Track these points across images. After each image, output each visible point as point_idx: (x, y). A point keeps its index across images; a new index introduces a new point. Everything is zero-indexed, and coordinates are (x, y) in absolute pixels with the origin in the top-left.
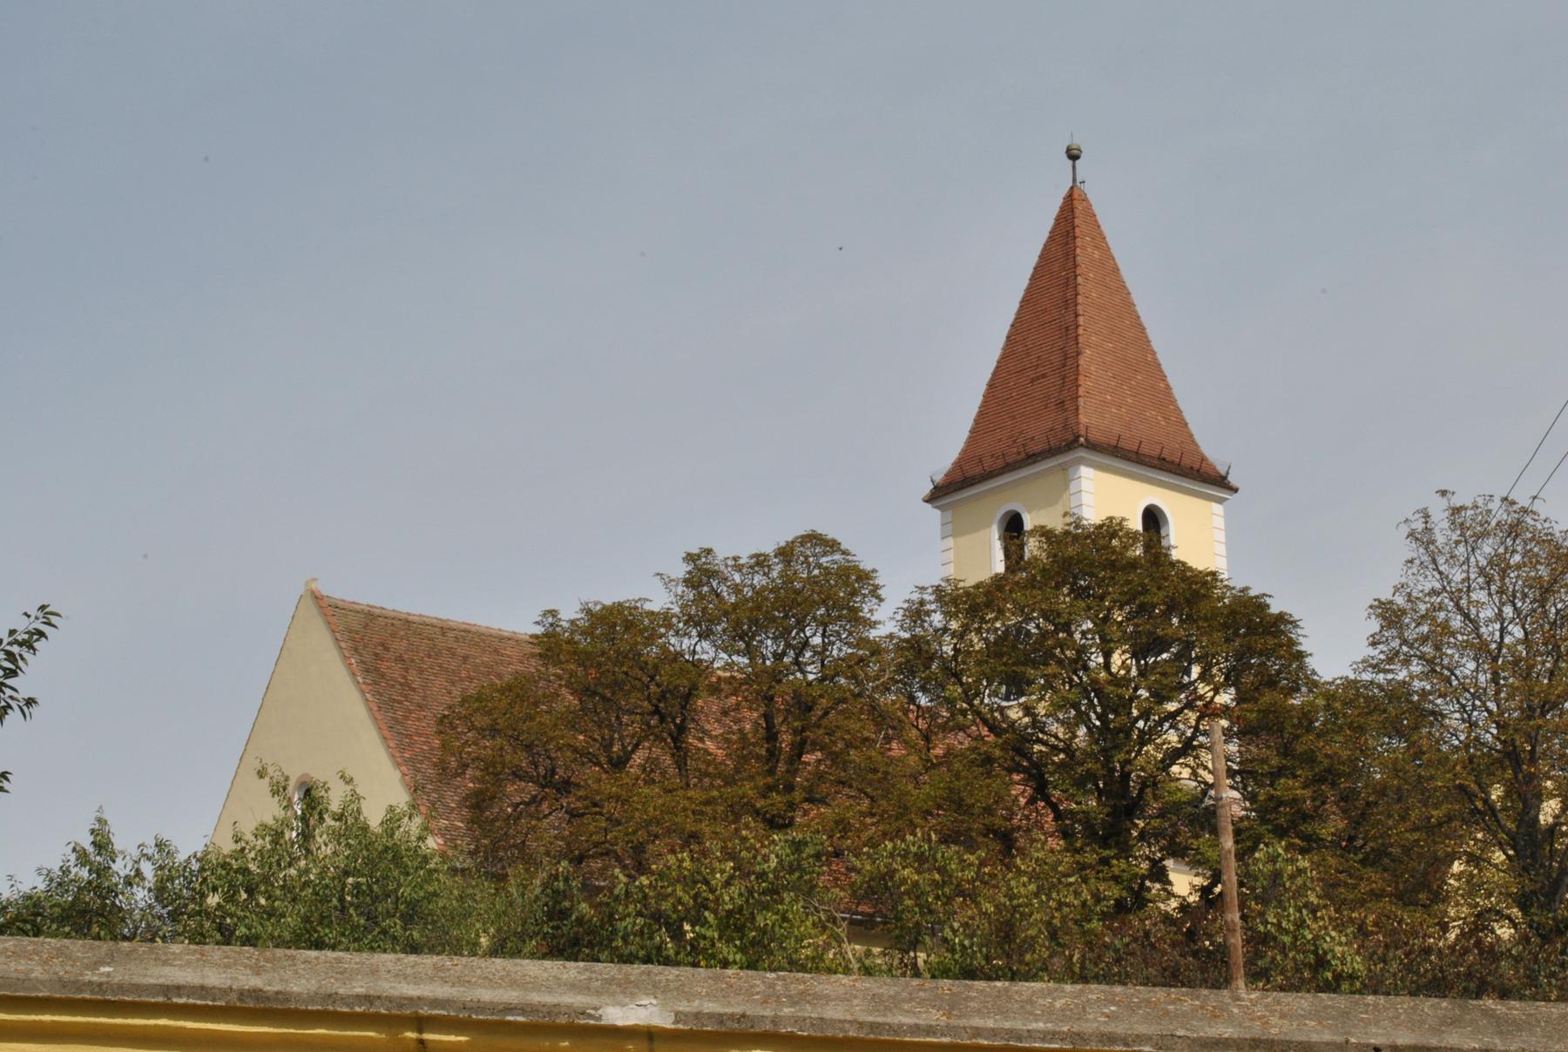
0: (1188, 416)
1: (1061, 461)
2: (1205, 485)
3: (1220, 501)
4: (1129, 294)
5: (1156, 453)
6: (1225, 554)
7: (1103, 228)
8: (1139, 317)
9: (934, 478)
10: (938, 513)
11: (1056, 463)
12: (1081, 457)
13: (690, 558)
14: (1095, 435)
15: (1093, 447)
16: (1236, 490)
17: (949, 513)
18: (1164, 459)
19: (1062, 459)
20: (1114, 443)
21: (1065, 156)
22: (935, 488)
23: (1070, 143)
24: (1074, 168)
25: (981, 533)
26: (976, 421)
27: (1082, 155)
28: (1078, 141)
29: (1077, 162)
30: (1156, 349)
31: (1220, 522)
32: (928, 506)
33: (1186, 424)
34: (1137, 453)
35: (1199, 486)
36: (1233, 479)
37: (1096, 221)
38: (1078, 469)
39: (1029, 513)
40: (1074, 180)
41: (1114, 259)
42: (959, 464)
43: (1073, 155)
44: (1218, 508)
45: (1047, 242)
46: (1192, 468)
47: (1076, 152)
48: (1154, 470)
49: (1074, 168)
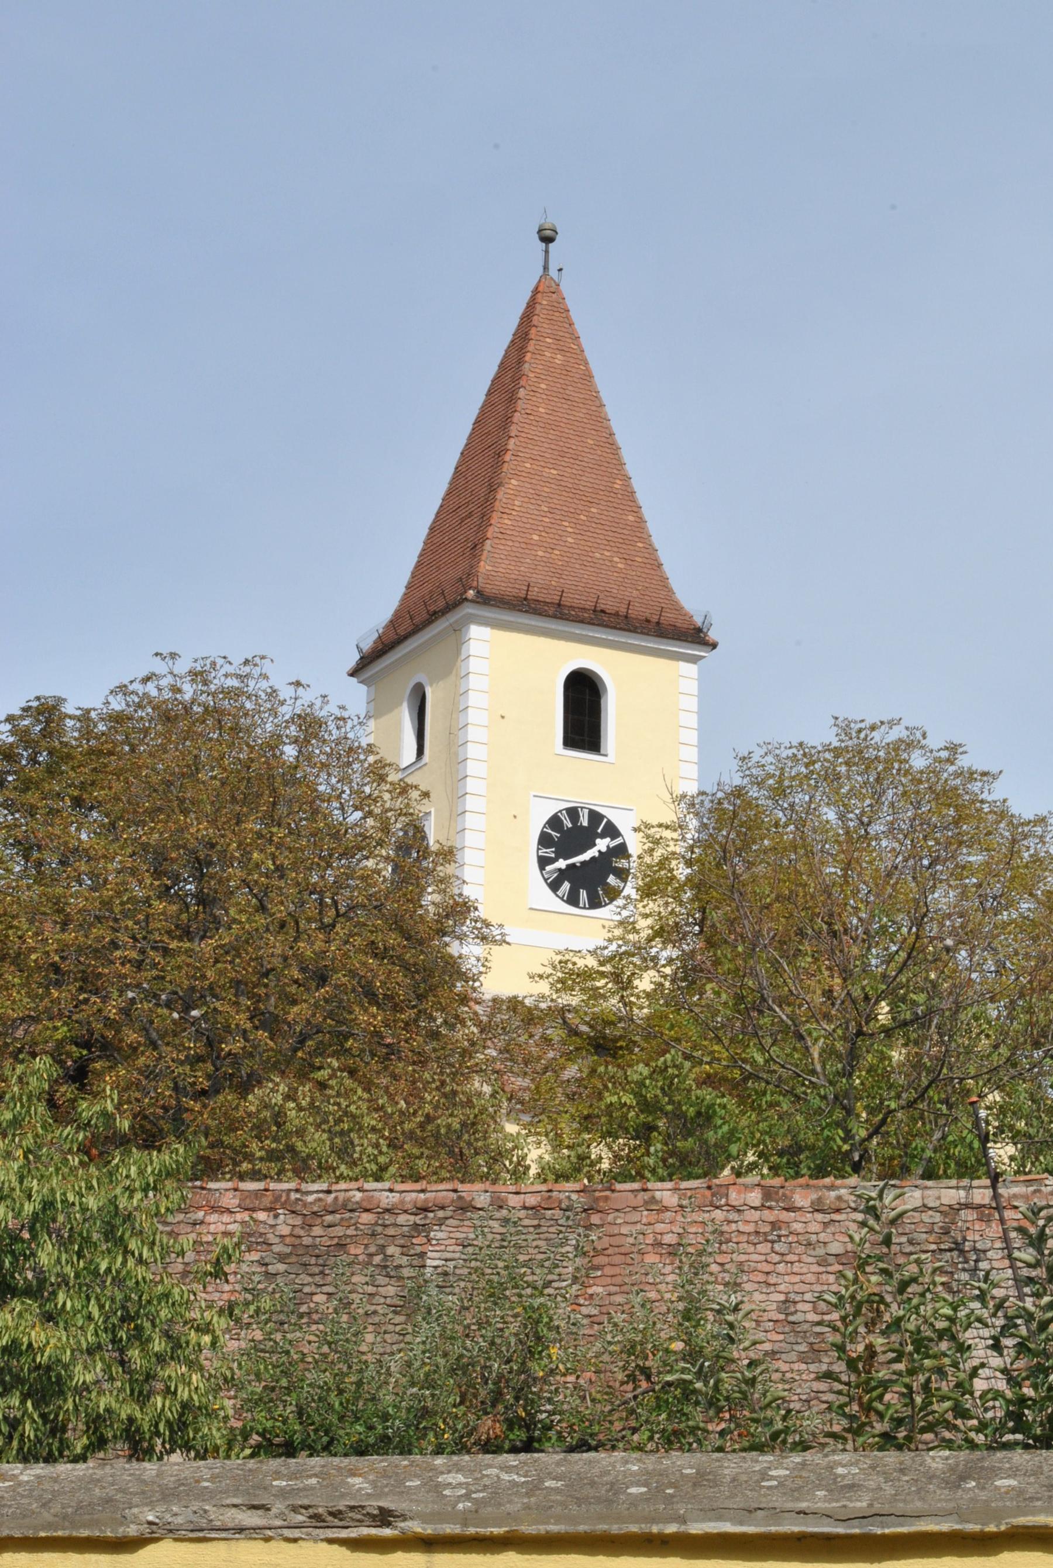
0: (665, 556)
1: (452, 620)
2: (665, 641)
3: (694, 660)
4: (602, 405)
5: (589, 605)
6: (696, 726)
7: (577, 326)
8: (612, 434)
9: (362, 645)
10: (363, 688)
11: (447, 623)
12: (471, 614)
13: (845, 728)
14: (489, 589)
15: (484, 599)
16: (714, 646)
17: (373, 688)
18: (603, 611)
19: (452, 618)
20: (523, 594)
21: (537, 236)
22: (361, 658)
23: (543, 221)
24: (547, 252)
25: (395, 712)
26: (414, 575)
27: (558, 238)
28: (551, 220)
29: (551, 245)
30: (631, 474)
31: (693, 687)
32: (354, 680)
33: (660, 565)
34: (559, 605)
35: (655, 643)
36: (713, 635)
37: (568, 317)
38: (468, 629)
39: (431, 686)
40: (546, 268)
41: (587, 363)
42: (393, 623)
43: (546, 237)
44: (690, 670)
45: (509, 347)
46: (648, 621)
47: (548, 233)
48: (581, 625)
49: (547, 252)
